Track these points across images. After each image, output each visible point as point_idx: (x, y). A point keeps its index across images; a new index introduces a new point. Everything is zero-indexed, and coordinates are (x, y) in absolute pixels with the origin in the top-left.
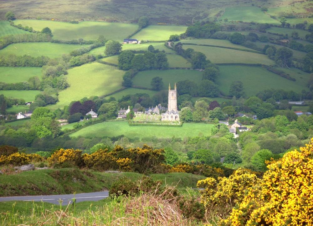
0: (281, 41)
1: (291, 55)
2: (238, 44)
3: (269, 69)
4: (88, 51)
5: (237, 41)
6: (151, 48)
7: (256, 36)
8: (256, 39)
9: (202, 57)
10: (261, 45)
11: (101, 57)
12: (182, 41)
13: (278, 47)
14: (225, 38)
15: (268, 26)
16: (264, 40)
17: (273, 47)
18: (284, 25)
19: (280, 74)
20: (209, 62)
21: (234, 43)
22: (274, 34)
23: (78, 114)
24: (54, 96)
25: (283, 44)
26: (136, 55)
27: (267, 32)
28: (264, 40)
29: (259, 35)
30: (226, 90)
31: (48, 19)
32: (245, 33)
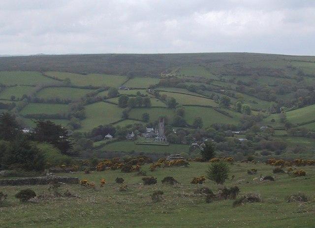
0: (221, 90)
1: (229, 101)
2: (193, 92)
3: (215, 109)
4: (97, 94)
5: (193, 90)
6: (138, 93)
7: (204, 87)
8: (204, 89)
9: (174, 101)
10: (210, 94)
11: (105, 98)
12: (158, 89)
13: (221, 96)
14: (185, 87)
15: (212, 80)
16: (210, 90)
17: (217, 95)
18: (56, 182)
19: (223, 113)
20: (178, 104)
21: (191, 91)
22: (51, 102)
23: (100, 136)
24: (78, 123)
25: (222, 93)
26: (130, 98)
27: (159, 179)
28: (210, 90)
29: (207, 86)
30: (191, 123)
31: (67, 71)
32: (198, 85)
